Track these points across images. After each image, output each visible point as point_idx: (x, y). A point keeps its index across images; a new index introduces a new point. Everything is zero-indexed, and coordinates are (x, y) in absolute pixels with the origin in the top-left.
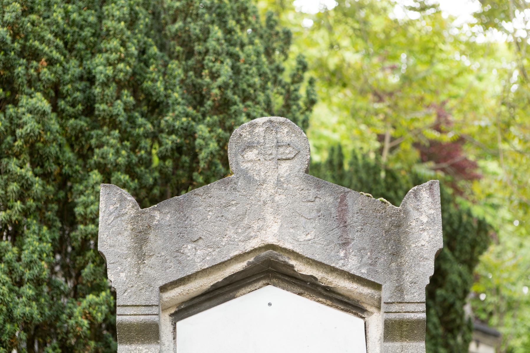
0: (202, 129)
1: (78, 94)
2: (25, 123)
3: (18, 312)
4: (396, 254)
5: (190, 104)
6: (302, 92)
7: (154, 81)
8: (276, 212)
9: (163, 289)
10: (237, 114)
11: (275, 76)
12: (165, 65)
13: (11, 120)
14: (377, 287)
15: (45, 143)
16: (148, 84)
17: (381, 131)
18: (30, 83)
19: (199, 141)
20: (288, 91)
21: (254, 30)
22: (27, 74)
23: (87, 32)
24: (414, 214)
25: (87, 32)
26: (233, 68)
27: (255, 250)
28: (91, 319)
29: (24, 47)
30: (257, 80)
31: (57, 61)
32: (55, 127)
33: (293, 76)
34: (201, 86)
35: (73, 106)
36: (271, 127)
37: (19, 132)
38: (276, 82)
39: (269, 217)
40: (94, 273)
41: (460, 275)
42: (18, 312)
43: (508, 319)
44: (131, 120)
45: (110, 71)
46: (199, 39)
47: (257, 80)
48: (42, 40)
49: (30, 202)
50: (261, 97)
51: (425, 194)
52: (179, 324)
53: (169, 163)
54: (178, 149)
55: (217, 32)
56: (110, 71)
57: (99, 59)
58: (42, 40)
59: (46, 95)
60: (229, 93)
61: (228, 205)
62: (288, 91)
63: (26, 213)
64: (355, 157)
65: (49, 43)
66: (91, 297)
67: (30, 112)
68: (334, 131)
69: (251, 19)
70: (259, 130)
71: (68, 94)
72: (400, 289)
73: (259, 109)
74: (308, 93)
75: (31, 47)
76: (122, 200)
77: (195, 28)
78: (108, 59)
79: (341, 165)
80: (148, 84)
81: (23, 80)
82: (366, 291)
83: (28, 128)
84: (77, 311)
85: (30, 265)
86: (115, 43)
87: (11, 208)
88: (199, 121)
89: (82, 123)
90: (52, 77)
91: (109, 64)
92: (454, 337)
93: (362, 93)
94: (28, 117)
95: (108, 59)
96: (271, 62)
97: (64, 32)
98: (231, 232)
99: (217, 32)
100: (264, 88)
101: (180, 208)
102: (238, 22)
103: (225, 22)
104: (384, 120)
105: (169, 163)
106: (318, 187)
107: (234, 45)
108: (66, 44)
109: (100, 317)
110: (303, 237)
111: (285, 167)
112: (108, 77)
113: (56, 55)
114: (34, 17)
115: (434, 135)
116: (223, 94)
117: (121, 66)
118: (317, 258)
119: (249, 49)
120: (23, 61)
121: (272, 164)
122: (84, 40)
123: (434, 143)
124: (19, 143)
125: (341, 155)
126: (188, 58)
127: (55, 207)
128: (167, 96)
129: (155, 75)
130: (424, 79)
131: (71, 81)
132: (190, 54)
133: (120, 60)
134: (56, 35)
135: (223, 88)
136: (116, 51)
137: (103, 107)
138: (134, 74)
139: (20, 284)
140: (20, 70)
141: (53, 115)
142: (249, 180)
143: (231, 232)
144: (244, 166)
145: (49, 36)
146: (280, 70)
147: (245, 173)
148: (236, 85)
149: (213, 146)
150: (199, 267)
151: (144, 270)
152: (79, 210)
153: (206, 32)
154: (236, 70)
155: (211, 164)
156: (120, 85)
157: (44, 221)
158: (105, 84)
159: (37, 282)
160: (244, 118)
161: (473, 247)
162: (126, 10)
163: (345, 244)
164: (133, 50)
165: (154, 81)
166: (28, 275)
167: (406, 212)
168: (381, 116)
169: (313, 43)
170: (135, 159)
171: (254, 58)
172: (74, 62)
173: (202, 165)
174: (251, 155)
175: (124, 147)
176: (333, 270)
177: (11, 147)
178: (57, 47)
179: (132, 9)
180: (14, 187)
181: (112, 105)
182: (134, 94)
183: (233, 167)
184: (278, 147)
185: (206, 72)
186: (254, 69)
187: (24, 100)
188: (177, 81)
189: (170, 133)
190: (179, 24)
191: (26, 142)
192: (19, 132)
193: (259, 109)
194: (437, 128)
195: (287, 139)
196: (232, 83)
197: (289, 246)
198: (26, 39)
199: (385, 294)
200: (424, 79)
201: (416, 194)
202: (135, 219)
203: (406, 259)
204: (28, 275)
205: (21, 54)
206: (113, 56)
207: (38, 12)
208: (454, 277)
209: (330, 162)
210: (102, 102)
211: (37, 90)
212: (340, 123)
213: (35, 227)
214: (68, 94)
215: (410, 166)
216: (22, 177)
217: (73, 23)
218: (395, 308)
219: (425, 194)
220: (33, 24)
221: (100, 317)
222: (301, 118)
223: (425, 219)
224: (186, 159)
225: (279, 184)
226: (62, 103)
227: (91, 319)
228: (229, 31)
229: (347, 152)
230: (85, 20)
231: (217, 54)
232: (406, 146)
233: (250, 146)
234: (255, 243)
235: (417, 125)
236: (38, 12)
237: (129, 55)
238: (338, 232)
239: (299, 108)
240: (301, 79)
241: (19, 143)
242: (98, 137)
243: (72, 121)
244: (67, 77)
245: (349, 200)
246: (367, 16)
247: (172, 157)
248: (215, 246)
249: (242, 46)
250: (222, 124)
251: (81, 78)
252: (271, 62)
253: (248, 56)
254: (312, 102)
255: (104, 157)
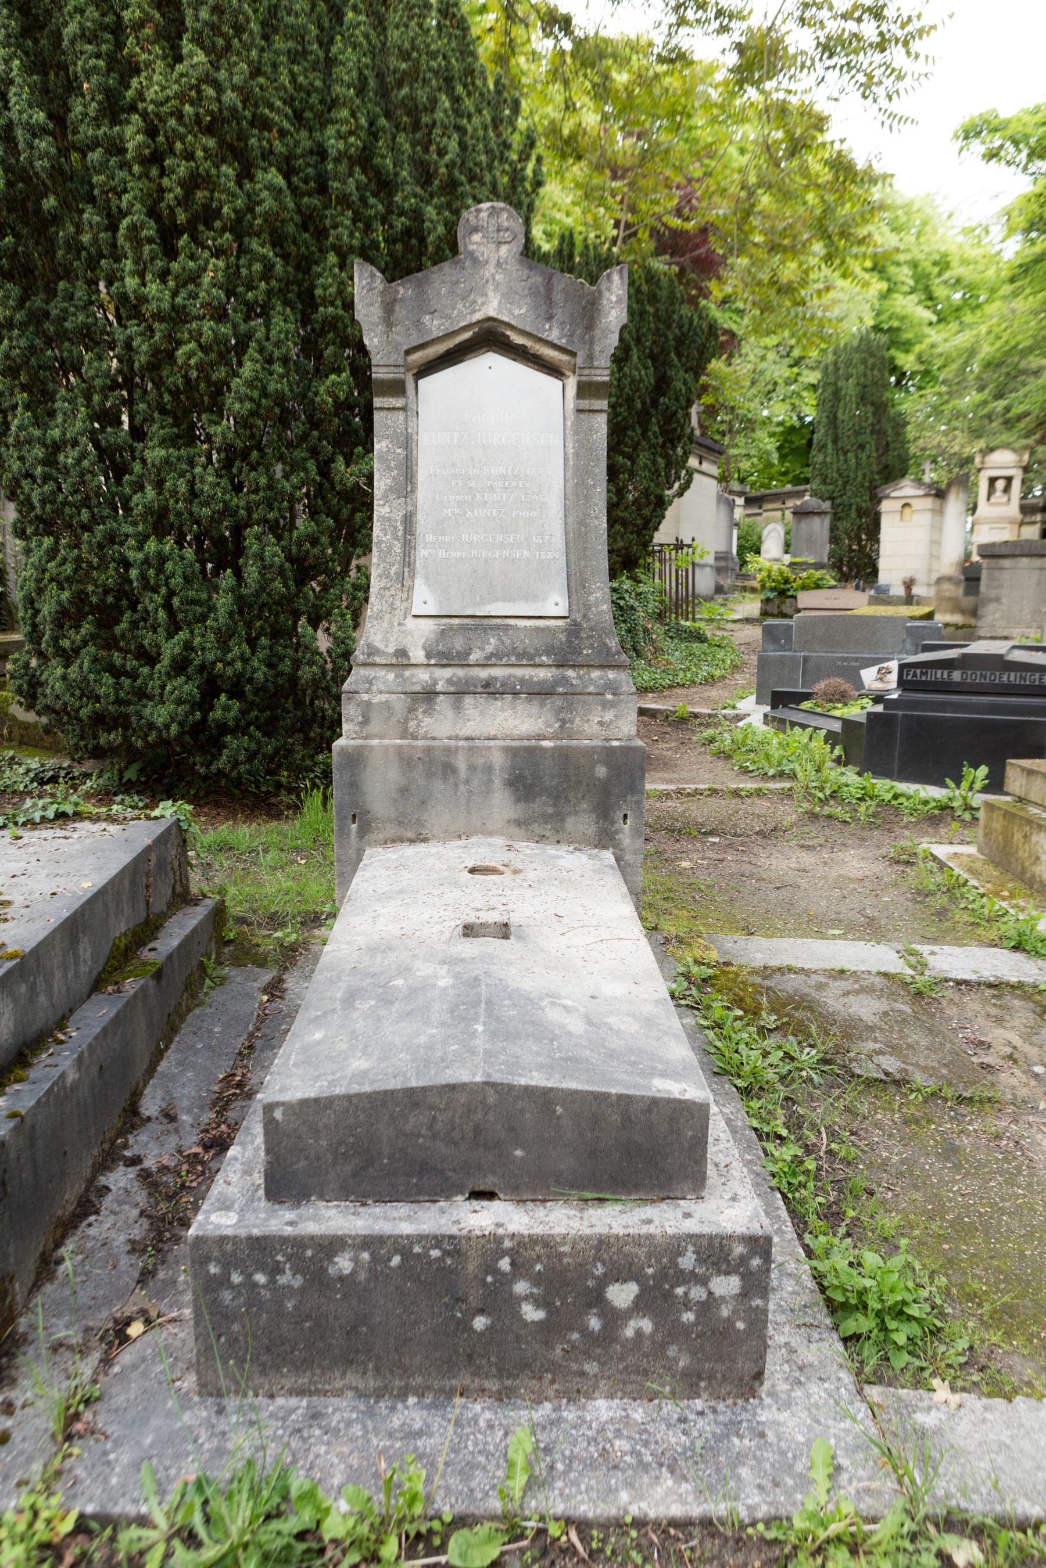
0: (430, 211)
1: (310, 170)
2: (263, 201)
3: (271, 387)
4: (590, 327)
5: (418, 183)
6: (529, 171)
7: (383, 157)
8: (496, 289)
9: (408, 352)
10: (463, 196)
11: (502, 154)
12: (394, 139)
13: (249, 196)
14: (573, 354)
15: (283, 221)
16: (377, 160)
17: (619, 215)
18: (264, 157)
19: (427, 224)
20: (515, 170)
21: (482, 95)
22: (261, 147)
23: (314, 99)
24: (607, 294)
25: (314, 99)
26: (460, 144)
27: (479, 322)
28: (334, 396)
29: (254, 115)
30: (483, 158)
31: (288, 132)
32: (292, 205)
33: (521, 153)
34: (428, 164)
35: (306, 182)
36: (494, 212)
37: (258, 209)
38: (503, 159)
39: (491, 294)
40: (335, 355)
41: (685, 383)
42: (271, 387)
43: (740, 440)
44: (363, 200)
45: (341, 145)
46: (426, 109)
47: (483, 158)
48: (271, 107)
49: (273, 283)
50: (488, 178)
51: (616, 277)
52: (421, 382)
53: (399, 247)
54: (408, 232)
55: (445, 102)
56: (341, 145)
57: (331, 130)
58: (271, 107)
59: (279, 170)
60: (456, 173)
61: (458, 282)
62: (515, 170)
63: (269, 293)
64: (587, 247)
65: (278, 111)
66: (333, 377)
67: (267, 188)
68: (568, 214)
69: (478, 83)
70: (484, 215)
71: (300, 170)
72: (590, 357)
73: (485, 192)
74: (534, 172)
75: (262, 115)
76: (372, 276)
77: (422, 95)
78: (338, 131)
79: (571, 256)
80: (377, 160)
81: (257, 153)
82: (565, 358)
83: (266, 205)
84: (322, 389)
85: (278, 344)
86: (345, 113)
87: (256, 288)
88: (428, 202)
89: (316, 201)
90: (284, 150)
91: (340, 136)
92: (674, 448)
93: (598, 168)
94: (265, 193)
95: (338, 131)
96: (499, 135)
97: (293, 99)
98: (460, 306)
99: (445, 102)
100: (490, 167)
101: (419, 284)
102: (465, 86)
103: (453, 89)
104: (622, 202)
105: (399, 247)
106: (531, 268)
107: (462, 116)
108: (295, 111)
109: (342, 396)
110: (517, 312)
111: (504, 250)
112: (339, 152)
113: (286, 125)
114: (261, 80)
115: (676, 222)
116: (450, 175)
117: (352, 139)
118: (528, 329)
119: (476, 120)
120: (255, 131)
121: (492, 247)
122: (311, 108)
123: (676, 233)
124: (258, 221)
125: (572, 244)
126: (414, 132)
127: (295, 288)
128: (396, 174)
129: (384, 151)
130: (667, 151)
131: (303, 156)
132: (416, 126)
133: (351, 133)
134: (285, 102)
135: (451, 166)
136: (347, 122)
137: (336, 184)
138: (364, 148)
139: (270, 361)
140: (253, 141)
141: (288, 193)
142: (475, 261)
143: (460, 306)
144: (471, 247)
145: (278, 103)
146: (507, 146)
147: (471, 255)
148: (463, 163)
149: (441, 229)
150: (436, 334)
151: (392, 336)
152: (318, 292)
153: (434, 102)
154: (462, 145)
155: (438, 248)
156: (352, 161)
157: (286, 303)
158: (337, 160)
159: (285, 360)
160: (470, 201)
161: (701, 353)
162: (355, 74)
163: (550, 318)
164: (363, 121)
165: (383, 157)
166: (277, 354)
167: (600, 292)
168: (619, 198)
169: (547, 100)
170: (367, 242)
171: (481, 133)
172: (304, 134)
173: (430, 249)
174: (477, 237)
175: (357, 229)
176: (540, 340)
177: (251, 225)
178: (286, 116)
179: (361, 73)
180: (257, 267)
181: (345, 183)
182: (364, 171)
183: (461, 249)
184: (499, 230)
185: (433, 148)
186: (481, 146)
187: (260, 175)
188: (405, 157)
189: (400, 215)
190: (405, 91)
191: (265, 221)
192: (258, 209)
193: (485, 192)
194: (679, 213)
195: (506, 224)
196: (459, 161)
197: (506, 319)
198: (256, 106)
199: (579, 361)
200: (667, 151)
201: (609, 276)
202: (383, 293)
203: (597, 332)
204: (277, 354)
205: (252, 124)
206: (344, 128)
207: (264, 74)
208: (679, 385)
209: (559, 252)
210: (335, 179)
211: (271, 165)
212: (574, 204)
213: (279, 308)
214: (300, 170)
215: (644, 260)
216: (264, 257)
217: (299, 88)
218: (586, 372)
219: (616, 277)
220: (261, 88)
221: (342, 396)
222: (526, 201)
223: (614, 299)
224: (414, 241)
225: (499, 264)
226: (295, 179)
227: (334, 396)
228: (456, 100)
229: (578, 239)
230: (311, 84)
231: (445, 127)
232: (644, 235)
233: (476, 230)
234: (478, 316)
235: (657, 209)
236: (264, 74)
237: (359, 127)
238: (544, 308)
239: (526, 191)
240: (528, 158)
241: (258, 221)
242: (333, 217)
243: (306, 199)
244: (299, 151)
245: (555, 281)
246: (609, 68)
247: (402, 240)
248: (448, 317)
249: (469, 117)
250: (448, 206)
251: (311, 152)
252: (499, 135)
253: (475, 130)
254: (538, 184)
255: (339, 238)
